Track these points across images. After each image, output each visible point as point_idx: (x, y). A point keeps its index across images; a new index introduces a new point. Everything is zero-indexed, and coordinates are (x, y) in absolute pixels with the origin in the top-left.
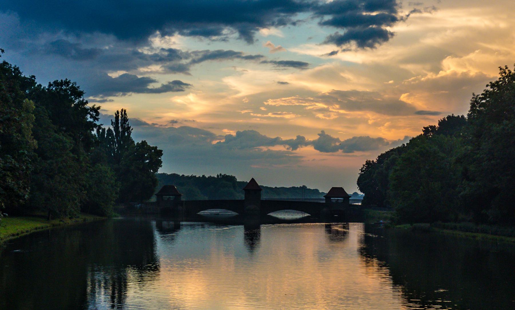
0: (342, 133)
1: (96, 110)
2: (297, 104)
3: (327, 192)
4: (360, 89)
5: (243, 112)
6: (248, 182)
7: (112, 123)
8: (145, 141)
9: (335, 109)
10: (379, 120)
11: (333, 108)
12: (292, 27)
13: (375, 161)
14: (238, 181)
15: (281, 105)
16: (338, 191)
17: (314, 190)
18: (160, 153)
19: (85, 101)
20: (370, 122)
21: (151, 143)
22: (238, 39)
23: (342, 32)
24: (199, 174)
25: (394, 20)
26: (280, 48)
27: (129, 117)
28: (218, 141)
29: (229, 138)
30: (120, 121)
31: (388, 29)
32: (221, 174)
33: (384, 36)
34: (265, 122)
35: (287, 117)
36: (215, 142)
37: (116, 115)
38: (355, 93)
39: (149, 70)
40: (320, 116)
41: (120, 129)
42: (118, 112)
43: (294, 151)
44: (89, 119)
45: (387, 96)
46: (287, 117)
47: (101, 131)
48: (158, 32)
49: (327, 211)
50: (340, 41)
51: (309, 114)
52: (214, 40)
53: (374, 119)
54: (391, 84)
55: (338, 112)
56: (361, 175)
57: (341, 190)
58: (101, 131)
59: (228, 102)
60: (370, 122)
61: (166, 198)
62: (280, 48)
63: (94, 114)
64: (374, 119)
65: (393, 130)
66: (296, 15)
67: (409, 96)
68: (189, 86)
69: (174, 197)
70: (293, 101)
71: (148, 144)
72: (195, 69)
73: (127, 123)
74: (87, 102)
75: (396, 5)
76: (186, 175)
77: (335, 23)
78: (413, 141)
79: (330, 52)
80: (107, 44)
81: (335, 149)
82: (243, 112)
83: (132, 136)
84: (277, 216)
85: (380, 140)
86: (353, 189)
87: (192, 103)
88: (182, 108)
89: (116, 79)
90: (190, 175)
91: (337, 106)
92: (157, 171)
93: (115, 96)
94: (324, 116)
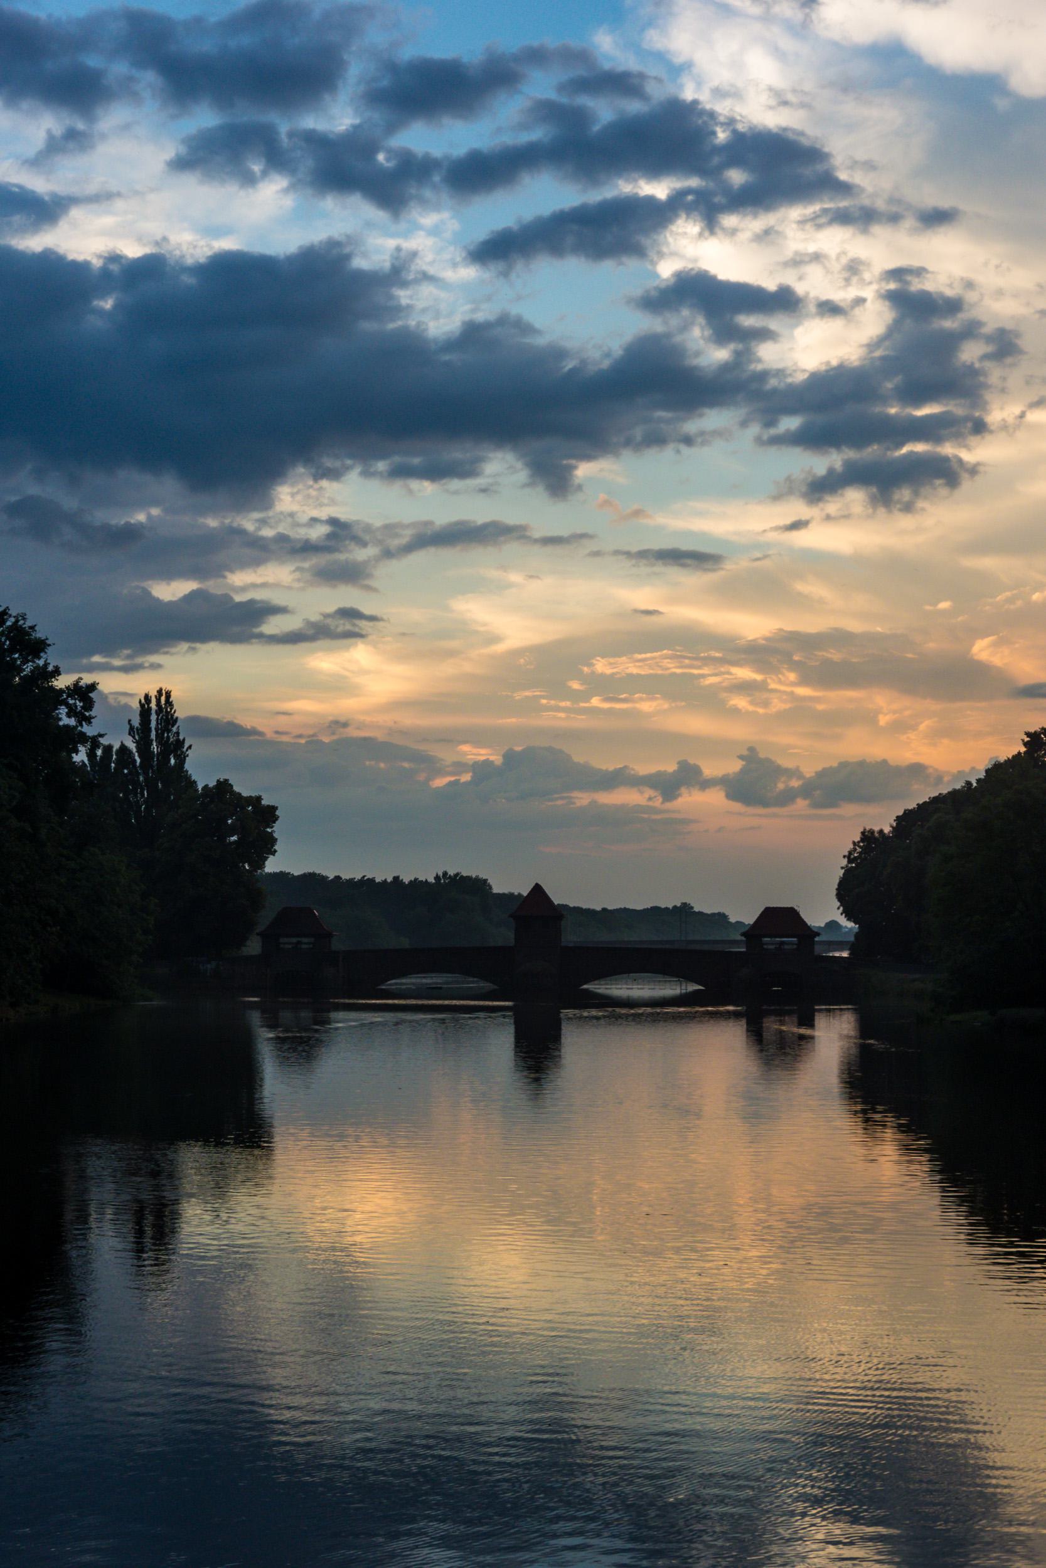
0: (804, 754)
1: (85, 693)
2: (678, 671)
3: (750, 919)
4: (855, 626)
5: (519, 695)
6: (525, 894)
7: (132, 728)
8: (226, 780)
9: (787, 684)
10: (907, 713)
11: (780, 682)
12: (683, 448)
13: (887, 830)
14: (495, 890)
15: (631, 675)
16: (780, 920)
17: (713, 915)
18: (269, 815)
19: (50, 668)
20: (883, 720)
21: (243, 788)
22: (525, 486)
23: (832, 460)
24: (382, 874)
25: (980, 428)
26: (637, 513)
27: (180, 712)
28: (453, 779)
29: (482, 770)
30: (153, 724)
31: (967, 456)
32: (445, 874)
33: (947, 473)
34: (580, 722)
35: (646, 706)
36: (440, 782)
37: (142, 706)
38: (839, 638)
39: (259, 581)
40: (741, 702)
41: (155, 748)
42: (147, 698)
43: (669, 805)
44: (66, 721)
45: (932, 645)
46: (646, 706)
47: (99, 752)
48: (301, 470)
49: (754, 977)
50: (819, 489)
51: (710, 700)
52: (456, 493)
53: (894, 712)
54: (943, 612)
55: (792, 693)
56: (848, 871)
57: (791, 914)
58: (99, 752)
59: (468, 668)
60: (883, 720)
61: (288, 942)
62: (637, 513)
63: (79, 704)
64: (894, 712)
65: (946, 741)
66: (701, 416)
67: (995, 645)
68: (381, 624)
69: (312, 940)
70: (667, 663)
71: (236, 789)
72: (387, 573)
73: (174, 729)
74: (57, 672)
75: (986, 386)
76: (345, 876)
77: (812, 439)
78: (997, 771)
79: (788, 521)
80: (150, 506)
81: (787, 798)
82: (519, 695)
83: (188, 766)
84: (608, 992)
85: (917, 770)
86: (823, 911)
87: (365, 672)
88: (339, 685)
89: (170, 604)
90: (358, 877)
91: (792, 676)
92: (262, 866)
93: (166, 653)
94: (752, 703)
